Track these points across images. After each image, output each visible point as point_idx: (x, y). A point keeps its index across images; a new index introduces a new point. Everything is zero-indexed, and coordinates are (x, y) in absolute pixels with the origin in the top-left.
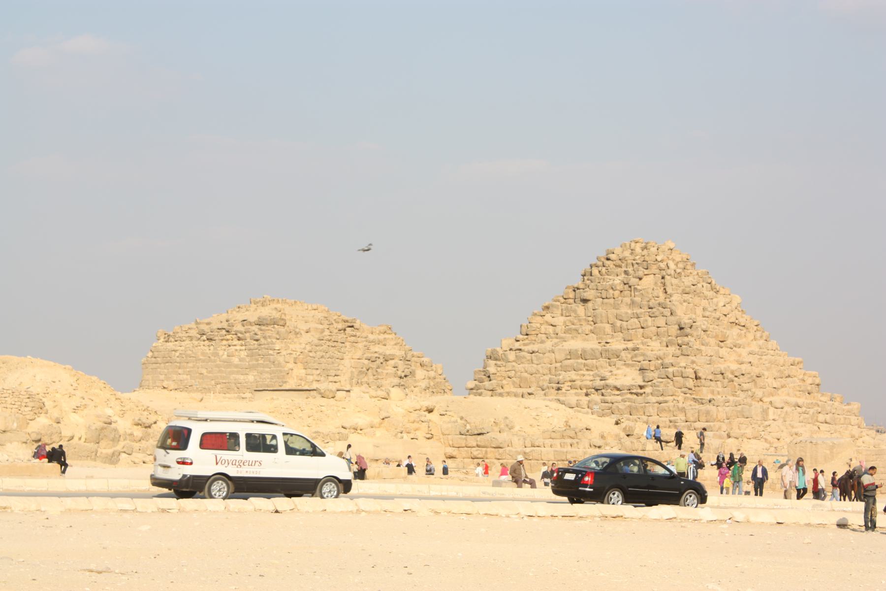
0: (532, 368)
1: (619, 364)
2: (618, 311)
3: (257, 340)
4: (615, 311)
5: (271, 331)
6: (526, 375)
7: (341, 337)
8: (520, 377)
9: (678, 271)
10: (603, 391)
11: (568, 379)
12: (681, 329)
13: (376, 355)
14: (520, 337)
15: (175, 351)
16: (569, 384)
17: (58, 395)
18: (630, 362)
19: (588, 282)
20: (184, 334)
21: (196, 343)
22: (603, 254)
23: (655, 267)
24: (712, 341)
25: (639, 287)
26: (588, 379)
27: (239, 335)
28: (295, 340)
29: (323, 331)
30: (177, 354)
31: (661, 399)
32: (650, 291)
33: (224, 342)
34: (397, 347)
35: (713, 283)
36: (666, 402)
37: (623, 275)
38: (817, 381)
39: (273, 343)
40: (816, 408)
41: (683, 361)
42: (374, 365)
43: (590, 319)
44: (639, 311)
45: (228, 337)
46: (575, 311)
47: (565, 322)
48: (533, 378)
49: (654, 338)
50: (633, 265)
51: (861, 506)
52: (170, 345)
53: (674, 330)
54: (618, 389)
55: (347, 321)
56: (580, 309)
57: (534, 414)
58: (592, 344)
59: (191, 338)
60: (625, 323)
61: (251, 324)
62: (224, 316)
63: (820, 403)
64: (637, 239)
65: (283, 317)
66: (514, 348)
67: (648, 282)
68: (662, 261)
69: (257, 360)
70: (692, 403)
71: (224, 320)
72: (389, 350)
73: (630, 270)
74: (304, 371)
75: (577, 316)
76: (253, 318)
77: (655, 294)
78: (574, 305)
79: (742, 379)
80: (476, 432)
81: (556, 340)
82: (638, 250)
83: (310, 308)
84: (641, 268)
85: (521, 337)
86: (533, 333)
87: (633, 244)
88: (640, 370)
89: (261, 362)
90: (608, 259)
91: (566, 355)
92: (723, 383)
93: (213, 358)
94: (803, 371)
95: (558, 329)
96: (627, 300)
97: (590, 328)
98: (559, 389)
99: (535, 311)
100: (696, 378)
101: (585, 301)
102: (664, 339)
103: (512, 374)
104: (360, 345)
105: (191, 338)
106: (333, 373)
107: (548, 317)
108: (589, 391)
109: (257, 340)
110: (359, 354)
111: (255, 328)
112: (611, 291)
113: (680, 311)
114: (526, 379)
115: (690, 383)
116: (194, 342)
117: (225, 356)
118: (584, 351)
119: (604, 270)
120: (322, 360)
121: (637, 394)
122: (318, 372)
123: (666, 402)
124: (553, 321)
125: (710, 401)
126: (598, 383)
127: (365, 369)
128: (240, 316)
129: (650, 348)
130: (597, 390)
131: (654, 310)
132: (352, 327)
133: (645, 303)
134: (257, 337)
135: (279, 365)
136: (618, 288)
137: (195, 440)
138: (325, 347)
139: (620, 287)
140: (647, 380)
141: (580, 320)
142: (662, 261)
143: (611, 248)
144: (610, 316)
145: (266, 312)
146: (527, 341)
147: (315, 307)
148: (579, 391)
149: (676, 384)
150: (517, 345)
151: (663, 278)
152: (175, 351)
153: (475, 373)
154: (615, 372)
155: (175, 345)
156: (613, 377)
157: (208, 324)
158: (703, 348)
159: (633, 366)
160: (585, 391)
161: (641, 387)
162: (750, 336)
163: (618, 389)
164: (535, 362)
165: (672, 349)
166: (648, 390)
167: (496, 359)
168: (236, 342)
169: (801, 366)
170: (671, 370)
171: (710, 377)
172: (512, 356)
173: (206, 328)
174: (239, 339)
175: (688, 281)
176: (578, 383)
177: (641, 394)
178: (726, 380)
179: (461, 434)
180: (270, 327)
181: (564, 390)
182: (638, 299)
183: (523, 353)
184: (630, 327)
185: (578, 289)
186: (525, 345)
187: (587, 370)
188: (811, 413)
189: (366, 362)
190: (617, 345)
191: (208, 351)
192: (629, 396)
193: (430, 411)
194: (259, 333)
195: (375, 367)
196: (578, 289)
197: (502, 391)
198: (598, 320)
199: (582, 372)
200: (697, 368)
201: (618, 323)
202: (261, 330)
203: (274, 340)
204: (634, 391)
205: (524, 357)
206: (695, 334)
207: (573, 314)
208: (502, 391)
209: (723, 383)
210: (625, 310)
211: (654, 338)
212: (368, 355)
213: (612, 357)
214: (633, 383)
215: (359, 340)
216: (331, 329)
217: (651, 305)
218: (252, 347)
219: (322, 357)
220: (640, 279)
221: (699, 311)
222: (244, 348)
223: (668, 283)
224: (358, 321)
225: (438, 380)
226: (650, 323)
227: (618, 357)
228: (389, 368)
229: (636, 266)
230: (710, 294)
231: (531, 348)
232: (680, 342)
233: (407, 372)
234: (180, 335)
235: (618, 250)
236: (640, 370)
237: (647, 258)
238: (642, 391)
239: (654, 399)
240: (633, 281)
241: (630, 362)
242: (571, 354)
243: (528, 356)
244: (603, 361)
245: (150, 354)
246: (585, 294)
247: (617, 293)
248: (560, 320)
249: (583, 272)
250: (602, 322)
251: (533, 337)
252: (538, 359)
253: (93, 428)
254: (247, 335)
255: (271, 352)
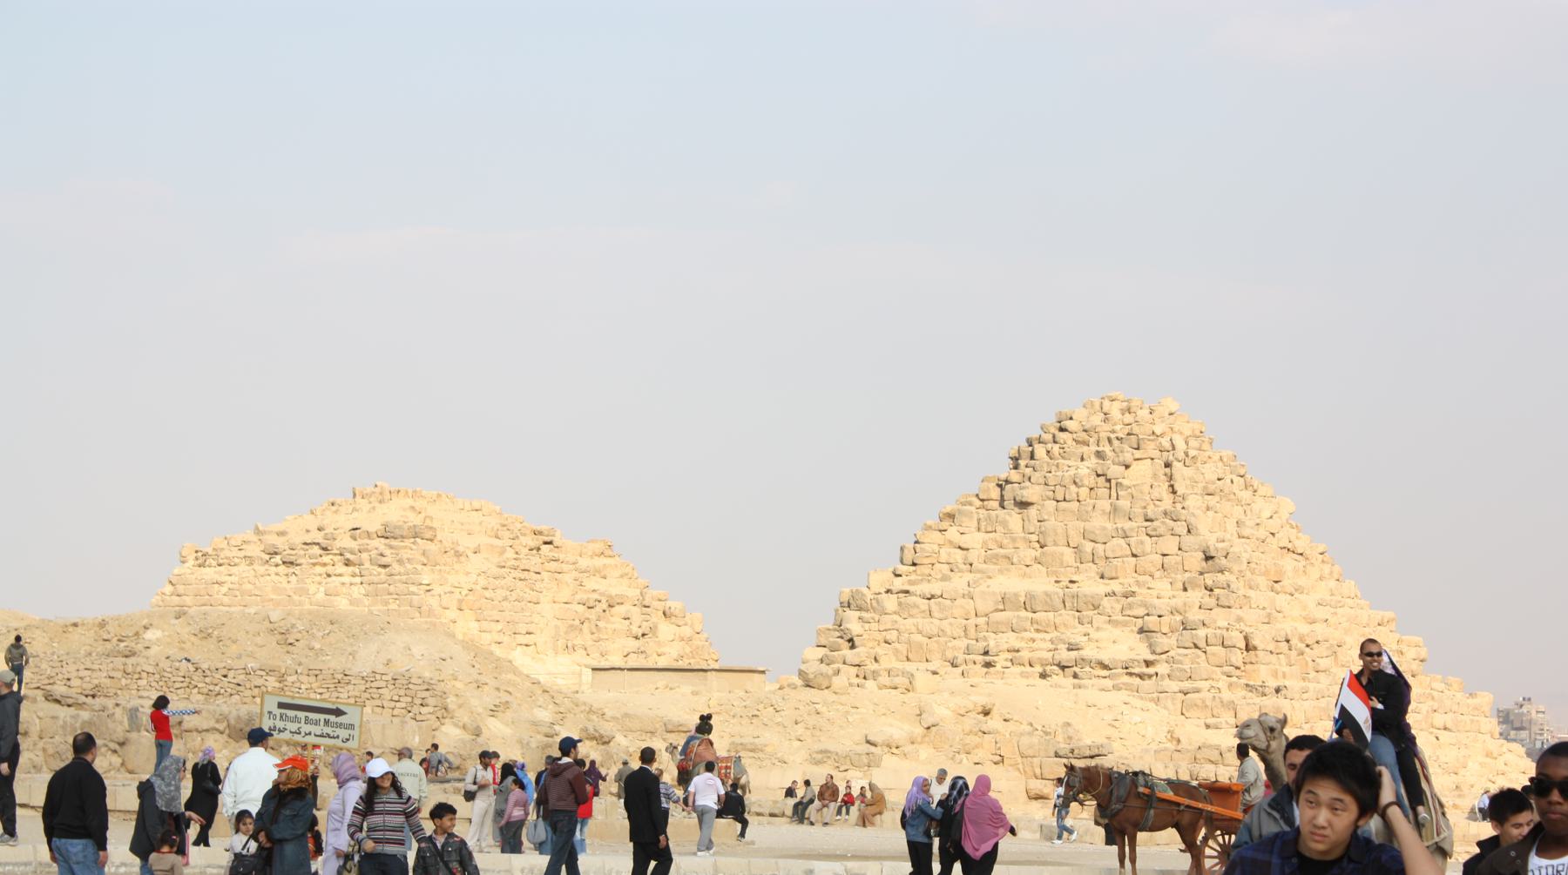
0: (931, 626)
1: (1099, 620)
2: (1088, 525)
3: (385, 566)
4: (1081, 524)
5: (409, 550)
6: (918, 638)
7: (534, 562)
8: (909, 642)
9: (1192, 453)
10: (1076, 669)
11: (1006, 647)
12: (1208, 558)
13: (596, 596)
14: (902, 569)
15: (220, 583)
16: (1009, 656)
17: (459, 685)
18: (1121, 618)
19: (1028, 471)
20: (235, 552)
21: (262, 569)
22: (1051, 421)
23: (1152, 445)
24: (1263, 582)
25: (1125, 482)
26: (1042, 648)
27: (348, 556)
28: (457, 566)
29: (503, 552)
30: (224, 589)
31: (1187, 685)
32: (1146, 488)
33: (319, 569)
34: (625, 581)
35: (1248, 476)
36: (1198, 691)
37: (1094, 460)
38: (1424, 653)
39: (416, 572)
40: (1431, 703)
41: (1221, 618)
42: (592, 614)
43: (1034, 538)
44: (1128, 525)
45: (326, 559)
46: (1004, 524)
47: (985, 543)
48: (933, 644)
49: (1157, 574)
50: (1109, 440)
51: (739, 826)
52: (209, 573)
53: (1195, 561)
54: (1106, 667)
55: (541, 533)
56: (1013, 518)
57: (1109, 717)
58: (1040, 584)
59: (250, 560)
60: (1100, 547)
61: (369, 535)
62: (312, 523)
63: (1435, 694)
64: (1113, 394)
65: (428, 522)
66: (895, 589)
67: (1142, 473)
68: (1162, 435)
69: (386, 603)
70: (1244, 693)
71: (313, 528)
72: (615, 587)
73: (1107, 449)
74: (475, 625)
75: (1008, 532)
76: (374, 526)
77: (1156, 495)
78: (1001, 512)
79: (1318, 650)
80: (1088, 753)
81: (970, 577)
82: (1115, 412)
83: (468, 507)
84: (1126, 447)
85: (905, 568)
86: (926, 561)
87: (1106, 403)
88: (1141, 631)
89: (393, 606)
90: (1062, 430)
91: (997, 603)
92: (1288, 657)
93: (296, 598)
94: (1397, 636)
95: (973, 556)
96: (1105, 504)
97: (1033, 553)
98: (988, 665)
99: (929, 522)
100: (1248, 649)
101: (1023, 505)
102: (1179, 577)
103: (892, 636)
104: (568, 578)
105: (250, 560)
106: (522, 628)
107: (953, 533)
108: (1048, 668)
109: (385, 566)
110: (565, 594)
111: (380, 544)
112: (1073, 487)
113: (1204, 524)
114: (920, 646)
115: (1238, 657)
116: (256, 566)
117: (321, 596)
118: (1031, 596)
119: (1056, 448)
120: (505, 604)
121: (1141, 676)
122: (500, 626)
123: (1198, 691)
124: (963, 541)
125: (1278, 691)
126: (1065, 656)
127: (577, 622)
128: (345, 521)
129: (1154, 593)
130: (1063, 668)
131: (1155, 523)
132: (550, 543)
133: (1138, 510)
134: (384, 561)
135: (430, 612)
136: (1086, 482)
137: (417, 758)
138: (509, 581)
139: (1091, 480)
140: (1159, 650)
141: (1014, 540)
142: (1162, 435)
143: (1066, 410)
144: (1071, 533)
145: (395, 512)
146: (913, 577)
147: (476, 505)
148: (1028, 669)
149: (1212, 659)
150: (898, 584)
151: (1167, 465)
152: (220, 583)
153: (819, 632)
154: (1094, 635)
155: (220, 573)
156: (1093, 645)
157: (282, 534)
158: (1251, 593)
159: (1125, 624)
160: (1038, 669)
161: (1148, 664)
162: (1314, 573)
163: (1106, 667)
164: (935, 614)
165: (1196, 596)
166: (1162, 668)
167: (860, 609)
168: (341, 569)
169: (1393, 626)
170: (1202, 632)
171: (1271, 647)
172: (890, 603)
173: (280, 543)
174: (348, 563)
175: (1210, 471)
176: (1025, 655)
177: (1150, 676)
178: (1294, 653)
179: (1057, 755)
180: (407, 543)
181: (998, 667)
182: (1124, 503)
183: (911, 599)
184: (1110, 554)
185: (1007, 482)
186: (911, 583)
187: (1038, 631)
188: (1424, 712)
189: (581, 608)
190: (1090, 585)
191: (285, 584)
192: (1126, 679)
193: (986, 713)
194: (388, 552)
195: (593, 617)
196: (1007, 482)
197: (875, 666)
198: (1049, 541)
199: (1027, 635)
200: (1248, 630)
201: (1088, 547)
202: (391, 547)
203: (419, 567)
204: (1136, 670)
205: (916, 606)
206: (1236, 568)
207: (999, 528)
208: (875, 666)
209: (1288, 657)
210: (1099, 523)
211: (1157, 574)
212: (581, 596)
213: (1083, 607)
214: (1133, 656)
215: (565, 567)
216: (518, 548)
217: (1151, 515)
218: (376, 579)
219: (505, 599)
220: (1127, 467)
221: (1231, 526)
222: (358, 580)
223: (1177, 476)
224: (558, 534)
225: (696, 643)
226: (1148, 548)
227: (1096, 607)
228: (615, 622)
229: (1116, 443)
230: (1246, 495)
231: (927, 588)
232: (1209, 583)
233: (645, 628)
234: (227, 553)
235: (1080, 414)
236: (1141, 631)
237: (1136, 429)
238: (1151, 670)
239: (1174, 686)
240: (1115, 471)
241: (1121, 618)
242: (1005, 601)
243: (923, 604)
244: (1067, 616)
245: (168, 589)
246: (1025, 492)
247: (1084, 492)
248: (974, 539)
249: (1014, 453)
250: (1055, 544)
251: (925, 570)
252: (942, 610)
253: (534, 745)
254: (365, 556)
255: (413, 588)
